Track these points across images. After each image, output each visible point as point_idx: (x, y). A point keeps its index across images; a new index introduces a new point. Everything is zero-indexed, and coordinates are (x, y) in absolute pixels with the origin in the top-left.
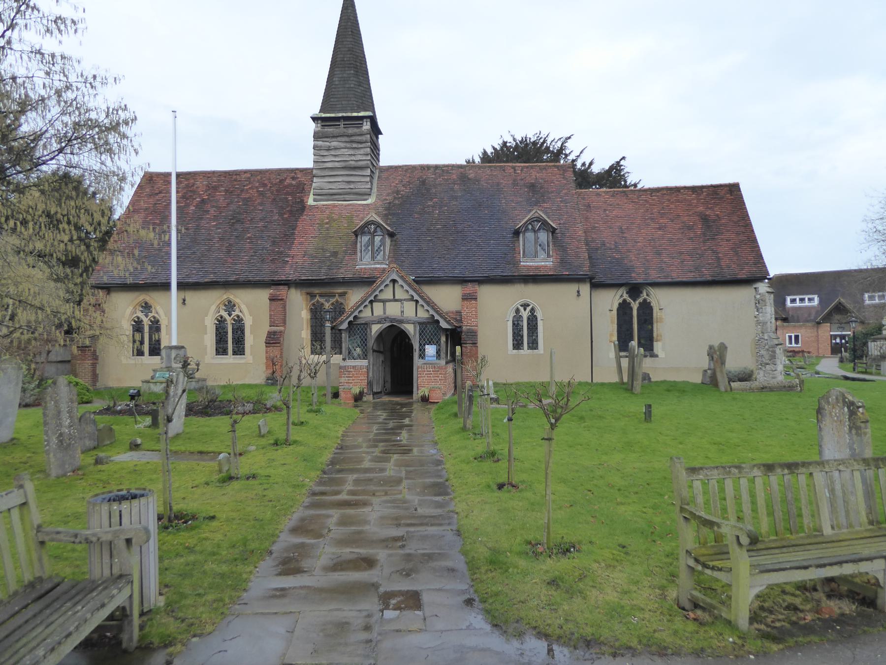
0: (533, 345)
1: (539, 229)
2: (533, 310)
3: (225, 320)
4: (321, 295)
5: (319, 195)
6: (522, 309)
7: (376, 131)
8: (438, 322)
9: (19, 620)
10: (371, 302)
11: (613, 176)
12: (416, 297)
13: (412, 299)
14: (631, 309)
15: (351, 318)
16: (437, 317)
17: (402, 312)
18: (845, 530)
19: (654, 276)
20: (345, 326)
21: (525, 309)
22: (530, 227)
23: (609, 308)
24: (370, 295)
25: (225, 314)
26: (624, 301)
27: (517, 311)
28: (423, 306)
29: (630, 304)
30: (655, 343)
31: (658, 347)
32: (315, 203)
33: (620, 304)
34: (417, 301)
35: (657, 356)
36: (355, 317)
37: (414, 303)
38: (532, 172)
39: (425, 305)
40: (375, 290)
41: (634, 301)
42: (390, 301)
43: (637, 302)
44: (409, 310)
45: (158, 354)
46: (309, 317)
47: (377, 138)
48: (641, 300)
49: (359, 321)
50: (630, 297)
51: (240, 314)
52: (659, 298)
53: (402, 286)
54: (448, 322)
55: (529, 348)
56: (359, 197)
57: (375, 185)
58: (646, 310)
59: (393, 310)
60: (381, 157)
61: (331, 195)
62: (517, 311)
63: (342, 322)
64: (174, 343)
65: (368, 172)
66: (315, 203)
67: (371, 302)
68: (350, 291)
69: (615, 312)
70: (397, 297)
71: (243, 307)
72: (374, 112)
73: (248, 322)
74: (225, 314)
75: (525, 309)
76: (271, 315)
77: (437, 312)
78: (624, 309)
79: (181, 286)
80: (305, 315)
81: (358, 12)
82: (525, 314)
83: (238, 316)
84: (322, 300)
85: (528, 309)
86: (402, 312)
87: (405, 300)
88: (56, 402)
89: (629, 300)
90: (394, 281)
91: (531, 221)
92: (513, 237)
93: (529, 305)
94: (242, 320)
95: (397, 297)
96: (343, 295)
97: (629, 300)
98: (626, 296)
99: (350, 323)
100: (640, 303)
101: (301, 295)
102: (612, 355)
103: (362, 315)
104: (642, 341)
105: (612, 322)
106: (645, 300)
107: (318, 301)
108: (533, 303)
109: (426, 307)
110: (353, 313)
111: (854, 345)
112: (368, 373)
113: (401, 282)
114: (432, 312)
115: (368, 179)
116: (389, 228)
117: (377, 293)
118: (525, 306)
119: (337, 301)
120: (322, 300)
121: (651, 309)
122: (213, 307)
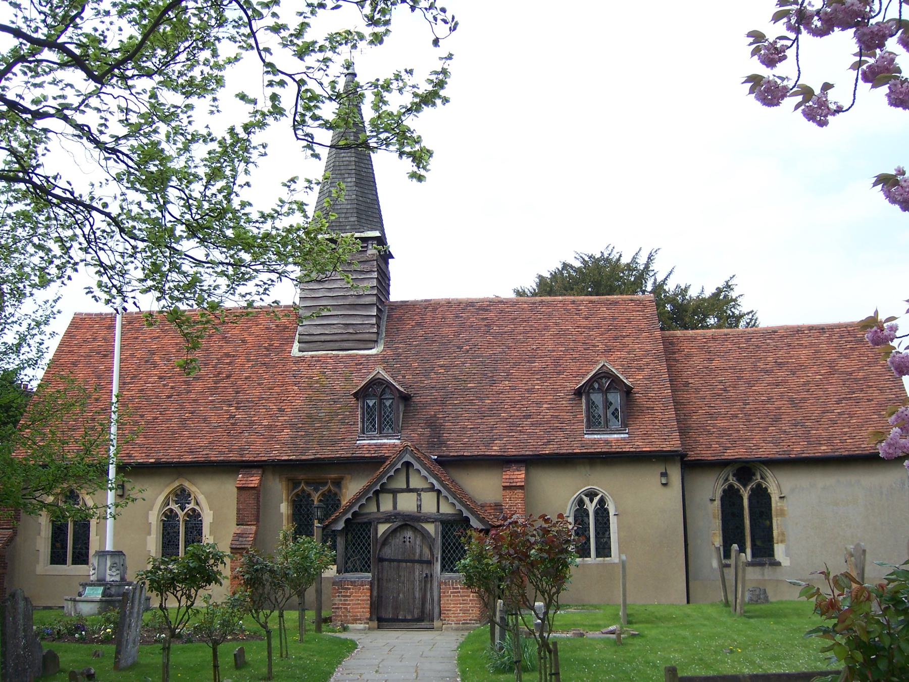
0: (604, 550)
1: (608, 389)
2: (602, 502)
3: (177, 515)
4: (308, 483)
5: (307, 343)
6: (586, 500)
7: (386, 256)
8: (467, 520)
9: (283, 641)
10: (377, 493)
11: (720, 304)
12: (437, 486)
13: (432, 489)
14: (741, 498)
15: (349, 516)
16: (466, 513)
17: (419, 506)
18: (301, 477)
19: (767, 451)
20: (340, 526)
21: (591, 501)
22: (596, 386)
23: (710, 497)
24: (375, 484)
25: (175, 507)
26: (731, 486)
27: (581, 502)
28: (446, 497)
29: (738, 490)
30: (775, 545)
31: (780, 552)
32: (301, 354)
33: (724, 491)
34: (439, 492)
35: (779, 564)
36: (354, 514)
37: (434, 494)
38: (603, 307)
39: (450, 497)
40: (381, 477)
41: (745, 486)
42: (402, 491)
43: (749, 488)
44: (429, 504)
45: (86, 562)
46: (290, 512)
47: (387, 263)
48: (752, 485)
49: (360, 520)
50: (739, 480)
51: (197, 508)
52: (777, 484)
53: (418, 471)
54: (482, 520)
55: (598, 555)
56: (362, 346)
57: (383, 329)
58: (761, 498)
59: (407, 503)
60: (392, 289)
61: (324, 344)
62: (581, 502)
63: (336, 520)
64: (109, 547)
65: (374, 312)
66: (301, 354)
67: (377, 493)
68: (349, 477)
69: (718, 503)
70: (411, 486)
71: (201, 498)
72: (382, 231)
73: (207, 518)
74: (175, 507)
75: (591, 501)
76: (238, 510)
77: (467, 507)
78: (730, 499)
79: (120, 469)
80: (284, 508)
81: (384, 222)
82: (591, 507)
83: (194, 510)
84: (308, 489)
85: (596, 500)
86: (419, 506)
87: (422, 490)
88: (14, 618)
89: (737, 485)
90: (408, 465)
91: (597, 377)
92: (573, 399)
93: (597, 495)
94: (199, 515)
95: (411, 486)
96: (338, 483)
97: (737, 485)
98: (732, 480)
99: (347, 521)
100: (752, 489)
101: (280, 481)
102: (715, 564)
103: (366, 510)
104: (758, 543)
105: (782, 513)
106: (759, 485)
107: (303, 491)
108: (602, 491)
109: (451, 500)
110: (351, 507)
111: (428, 519)
112: (371, 590)
113: (417, 466)
114: (459, 506)
115: (374, 321)
116: (402, 390)
117: (385, 480)
118: (591, 495)
119: (330, 491)
120: (308, 489)
121: (769, 497)
122: (161, 498)
